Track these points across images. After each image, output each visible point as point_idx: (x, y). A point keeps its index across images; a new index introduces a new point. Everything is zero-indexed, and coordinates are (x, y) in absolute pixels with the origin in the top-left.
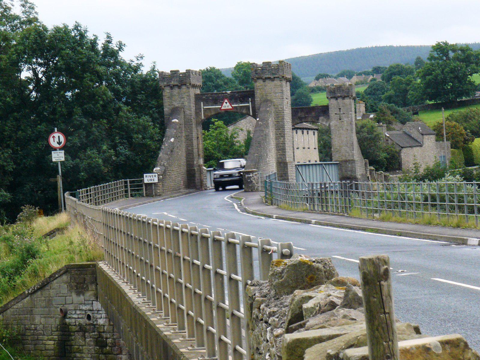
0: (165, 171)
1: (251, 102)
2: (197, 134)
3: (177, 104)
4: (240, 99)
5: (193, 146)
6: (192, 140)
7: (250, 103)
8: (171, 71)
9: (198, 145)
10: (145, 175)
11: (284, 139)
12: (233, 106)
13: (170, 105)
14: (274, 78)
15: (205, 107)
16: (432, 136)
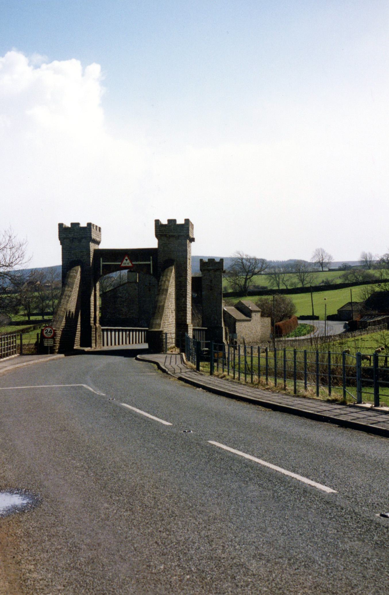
8: (72, 224)
12: (133, 263)
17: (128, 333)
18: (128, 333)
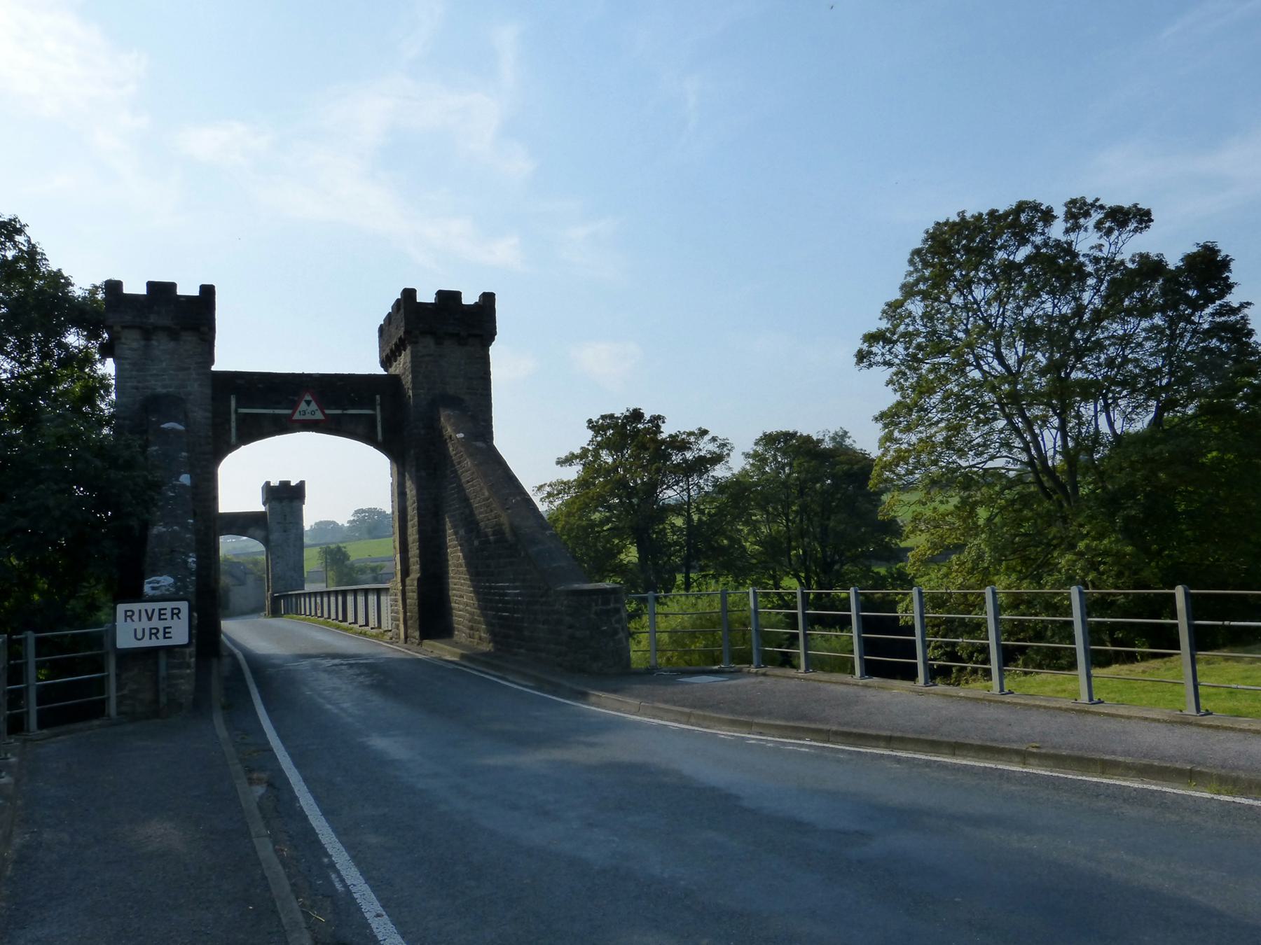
3: (164, 387)
7: (378, 408)
8: (151, 285)
12: (327, 412)
13: (137, 388)
17: (372, 599)
18: (372, 599)
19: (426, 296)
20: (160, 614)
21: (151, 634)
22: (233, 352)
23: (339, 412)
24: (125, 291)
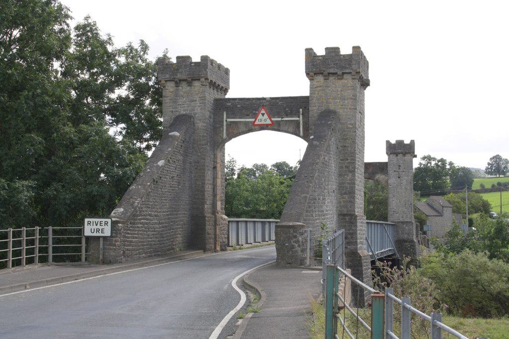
0: (134, 216)
1: (303, 114)
2: (214, 162)
3: (184, 111)
4: (285, 109)
5: (204, 180)
6: (204, 169)
7: (301, 116)
9: (214, 179)
10: (86, 220)
11: (354, 175)
12: (273, 119)
13: (172, 112)
14: (343, 73)
15: (229, 120)
16: (449, 209)
19: (320, 52)
20: (100, 224)
21: (97, 231)
22: (239, 88)
23: (280, 119)
24: (342, 53)
